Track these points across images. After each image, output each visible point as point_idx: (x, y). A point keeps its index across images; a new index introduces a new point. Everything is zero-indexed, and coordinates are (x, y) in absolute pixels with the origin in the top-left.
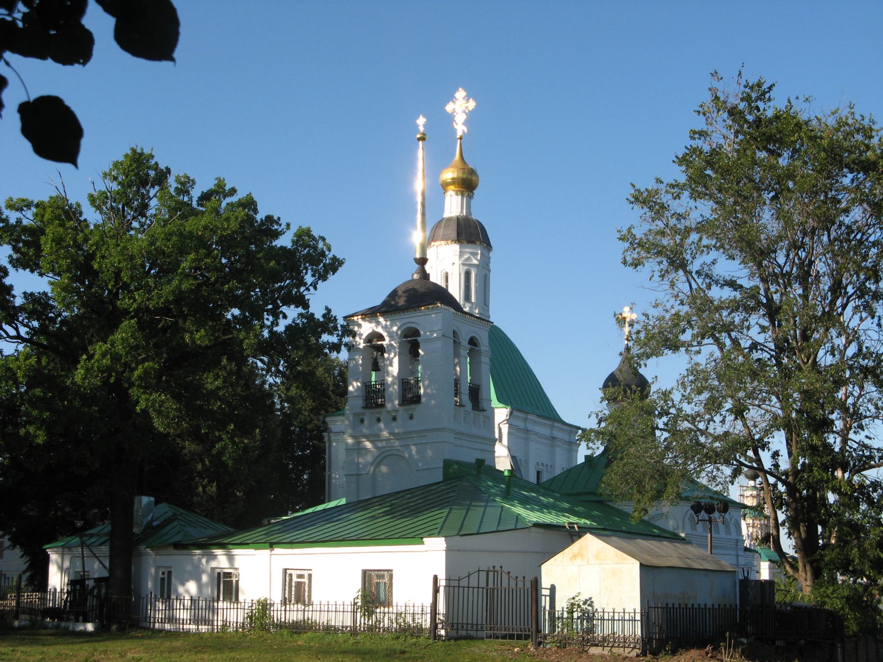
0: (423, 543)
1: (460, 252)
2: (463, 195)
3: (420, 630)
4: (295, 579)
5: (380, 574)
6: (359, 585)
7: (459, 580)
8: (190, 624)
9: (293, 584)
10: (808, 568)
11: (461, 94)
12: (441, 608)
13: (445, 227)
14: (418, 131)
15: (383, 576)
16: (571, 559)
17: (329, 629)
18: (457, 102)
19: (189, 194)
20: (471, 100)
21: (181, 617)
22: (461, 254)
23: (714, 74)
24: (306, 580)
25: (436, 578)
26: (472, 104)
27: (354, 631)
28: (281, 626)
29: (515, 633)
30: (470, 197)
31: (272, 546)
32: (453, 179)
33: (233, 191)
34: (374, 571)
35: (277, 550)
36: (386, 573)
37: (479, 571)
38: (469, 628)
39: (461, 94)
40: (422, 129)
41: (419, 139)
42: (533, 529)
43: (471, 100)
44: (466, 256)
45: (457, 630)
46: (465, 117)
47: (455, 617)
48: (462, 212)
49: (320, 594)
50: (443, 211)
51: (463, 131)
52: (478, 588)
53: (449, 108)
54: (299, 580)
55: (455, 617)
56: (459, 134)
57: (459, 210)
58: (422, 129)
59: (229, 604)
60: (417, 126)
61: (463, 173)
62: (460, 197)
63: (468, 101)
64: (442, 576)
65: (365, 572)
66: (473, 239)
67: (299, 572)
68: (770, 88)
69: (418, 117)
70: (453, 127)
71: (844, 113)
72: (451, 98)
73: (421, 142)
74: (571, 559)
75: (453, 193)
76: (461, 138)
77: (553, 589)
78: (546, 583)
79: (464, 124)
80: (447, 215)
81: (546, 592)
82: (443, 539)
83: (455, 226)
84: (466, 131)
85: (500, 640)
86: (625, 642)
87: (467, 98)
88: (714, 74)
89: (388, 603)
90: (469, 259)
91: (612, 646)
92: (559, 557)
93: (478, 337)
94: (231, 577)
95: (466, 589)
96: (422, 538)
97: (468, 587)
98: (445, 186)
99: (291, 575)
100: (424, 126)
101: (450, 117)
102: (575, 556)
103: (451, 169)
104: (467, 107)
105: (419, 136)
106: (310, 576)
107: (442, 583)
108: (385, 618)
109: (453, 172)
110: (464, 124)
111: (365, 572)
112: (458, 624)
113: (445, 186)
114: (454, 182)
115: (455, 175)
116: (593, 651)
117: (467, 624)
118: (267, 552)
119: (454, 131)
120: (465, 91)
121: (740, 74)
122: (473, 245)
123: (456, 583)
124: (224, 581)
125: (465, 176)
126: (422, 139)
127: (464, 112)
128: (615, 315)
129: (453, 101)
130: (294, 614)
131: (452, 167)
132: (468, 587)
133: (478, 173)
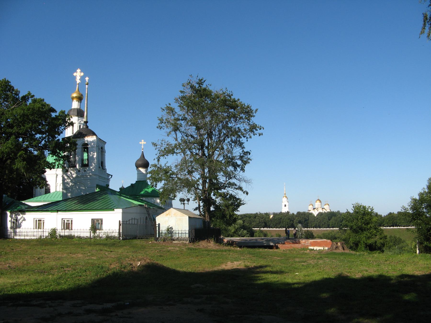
0: (114, 211)
1: (78, 119)
2: (78, 102)
3: (115, 237)
4: (66, 222)
5: (98, 220)
6: (91, 224)
7: (127, 222)
8: (30, 236)
9: (65, 223)
10: (208, 216)
11: (79, 70)
12: (121, 231)
13: (73, 111)
14: (86, 82)
15: (99, 221)
16: (166, 215)
17: (79, 238)
18: (78, 73)
19: (19, 95)
20: (82, 73)
21: (29, 234)
22: (78, 120)
23: (191, 76)
24: (70, 222)
25: (120, 221)
26: (82, 74)
27: (90, 238)
28: (60, 236)
29: (140, 237)
30: (81, 102)
31: (58, 211)
32: (76, 96)
33: (33, 96)
34: (96, 219)
35: (59, 213)
36: (100, 220)
37: (132, 219)
38: (130, 236)
39: (79, 70)
40: (87, 81)
41: (86, 84)
42: (139, 206)
43: (82, 73)
44: (80, 121)
45: (126, 237)
46: (80, 78)
47: (127, 233)
48: (78, 107)
49: (75, 226)
50: (72, 106)
51: (79, 82)
52: (134, 224)
53: (75, 74)
54: (67, 222)
55: (127, 233)
56: (78, 83)
57: (77, 106)
58: (87, 81)
59: (73, 234)
60: (86, 80)
61: (79, 95)
62: (78, 102)
63: (81, 73)
64: (121, 221)
65: (92, 219)
66: (82, 116)
67: (67, 220)
68: (204, 81)
69: (86, 77)
70: (76, 80)
71: (224, 90)
72: (76, 72)
73: (87, 85)
74: (166, 215)
75: (76, 101)
76: (78, 84)
77: (159, 224)
78: (157, 223)
79: (80, 80)
80: (73, 107)
81: (157, 226)
82: (121, 209)
83: (77, 111)
84: (80, 82)
85: (140, 240)
86: (184, 239)
87: (81, 72)
88: (191, 76)
89: (101, 229)
90: (81, 122)
91: (180, 241)
92: (162, 215)
93: (81, 144)
94: (41, 221)
95: (128, 225)
96: (114, 209)
97: (129, 224)
98: (73, 98)
99: (64, 221)
100: (88, 80)
101: (75, 77)
102: (167, 215)
103: (76, 93)
104: (81, 75)
105: (86, 83)
106: (72, 221)
107: (121, 223)
108: (101, 233)
109: (76, 94)
110: (80, 80)
111: (92, 219)
112: (126, 235)
113: (73, 98)
114: (76, 97)
115: (77, 95)
116: (174, 242)
117: (126, 235)
118: (56, 213)
119: (76, 82)
120: (80, 70)
121: (198, 76)
122: (82, 117)
123: (125, 223)
124: (38, 223)
125: (80, 96)
126: (87, 84)
127: (80, 76)
128: (152, 143)
129: (76, 73)
130: (67, 233)
131: (76, 93)
132: (129, 224)
133: (83, 95)
